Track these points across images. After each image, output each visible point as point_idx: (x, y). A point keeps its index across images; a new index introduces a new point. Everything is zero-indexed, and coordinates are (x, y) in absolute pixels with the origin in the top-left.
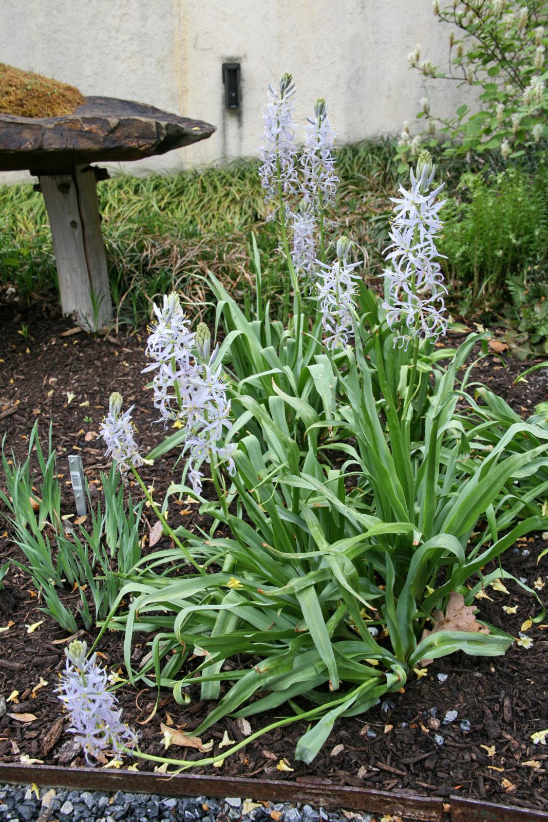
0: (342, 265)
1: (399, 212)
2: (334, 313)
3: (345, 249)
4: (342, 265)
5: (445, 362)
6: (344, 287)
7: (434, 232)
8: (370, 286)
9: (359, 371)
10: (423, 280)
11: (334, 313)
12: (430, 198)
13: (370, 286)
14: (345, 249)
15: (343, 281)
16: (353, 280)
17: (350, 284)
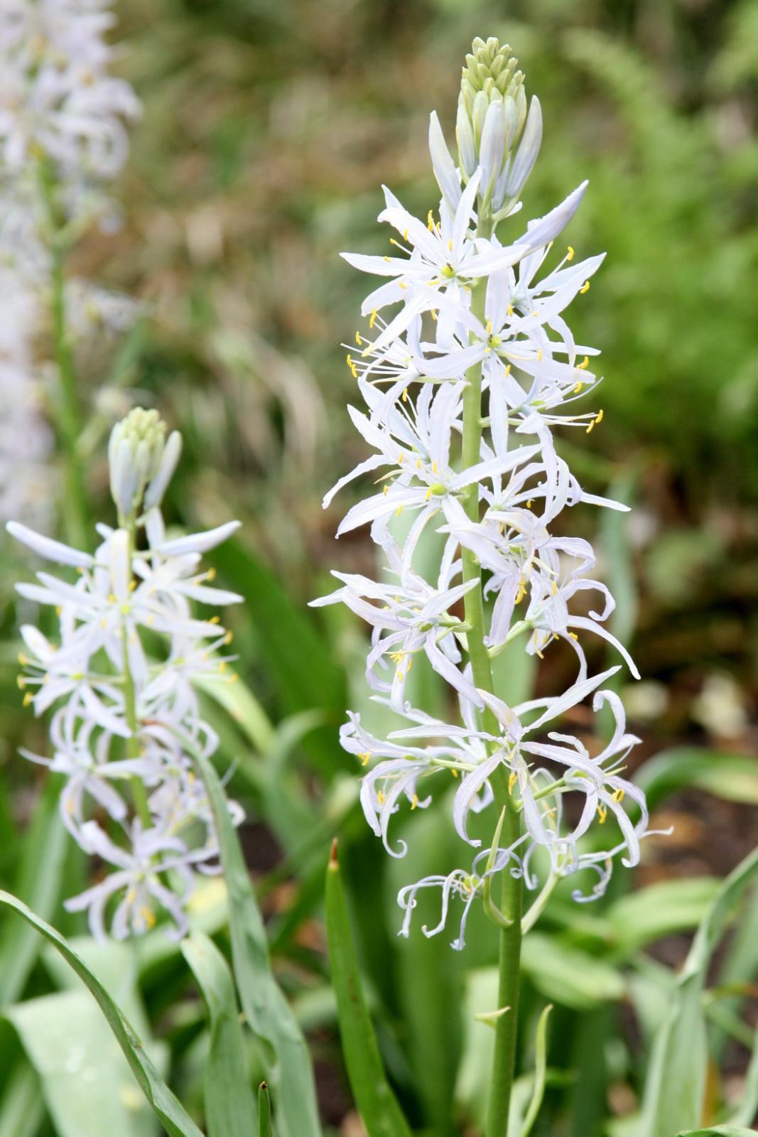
0: (142, 542)
1: (392, 311)
2: (120, 769)
3: (151, 469)
4: (142, 542)
5: (669, 947)
6: (158, 649)
7: (556, 399)
8: (290, 650)
9: (428, 501)
10: (521, 609)
11: (120, 769)
12: (529, 249)
13: (290, 650)
14: (151, 469)
15: (155, 623)
16: (203, 611)
17: (189, 634)
